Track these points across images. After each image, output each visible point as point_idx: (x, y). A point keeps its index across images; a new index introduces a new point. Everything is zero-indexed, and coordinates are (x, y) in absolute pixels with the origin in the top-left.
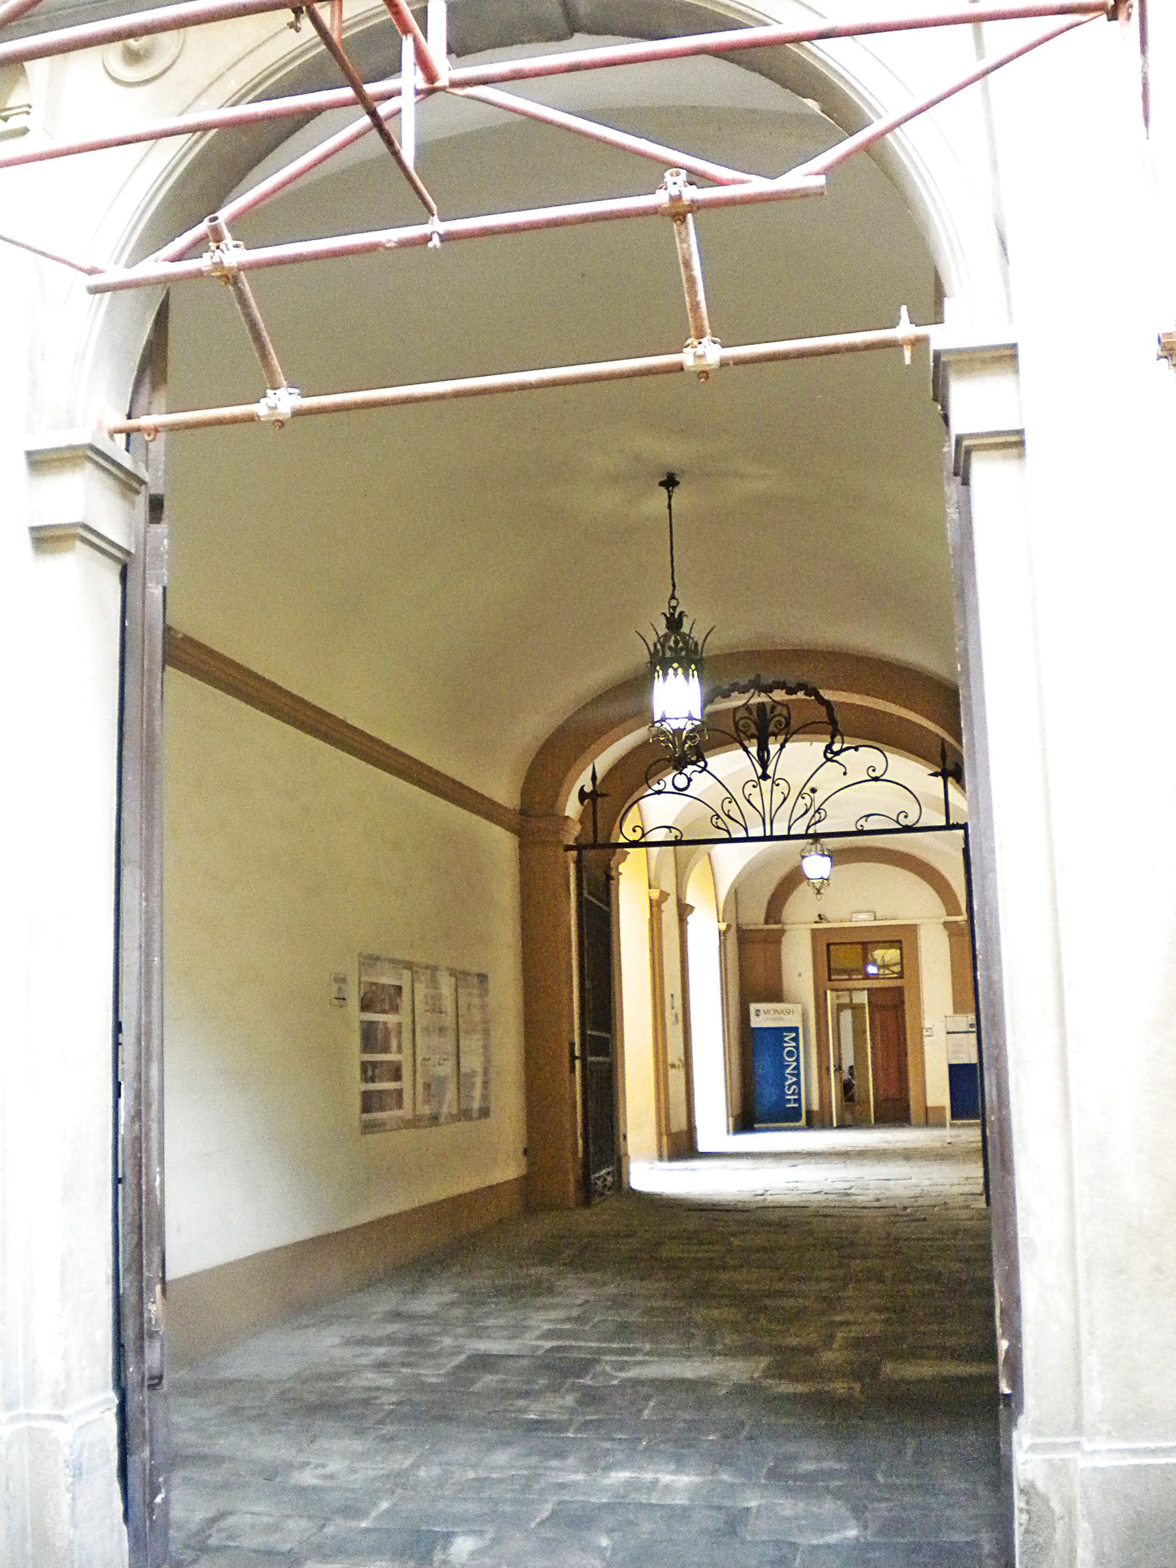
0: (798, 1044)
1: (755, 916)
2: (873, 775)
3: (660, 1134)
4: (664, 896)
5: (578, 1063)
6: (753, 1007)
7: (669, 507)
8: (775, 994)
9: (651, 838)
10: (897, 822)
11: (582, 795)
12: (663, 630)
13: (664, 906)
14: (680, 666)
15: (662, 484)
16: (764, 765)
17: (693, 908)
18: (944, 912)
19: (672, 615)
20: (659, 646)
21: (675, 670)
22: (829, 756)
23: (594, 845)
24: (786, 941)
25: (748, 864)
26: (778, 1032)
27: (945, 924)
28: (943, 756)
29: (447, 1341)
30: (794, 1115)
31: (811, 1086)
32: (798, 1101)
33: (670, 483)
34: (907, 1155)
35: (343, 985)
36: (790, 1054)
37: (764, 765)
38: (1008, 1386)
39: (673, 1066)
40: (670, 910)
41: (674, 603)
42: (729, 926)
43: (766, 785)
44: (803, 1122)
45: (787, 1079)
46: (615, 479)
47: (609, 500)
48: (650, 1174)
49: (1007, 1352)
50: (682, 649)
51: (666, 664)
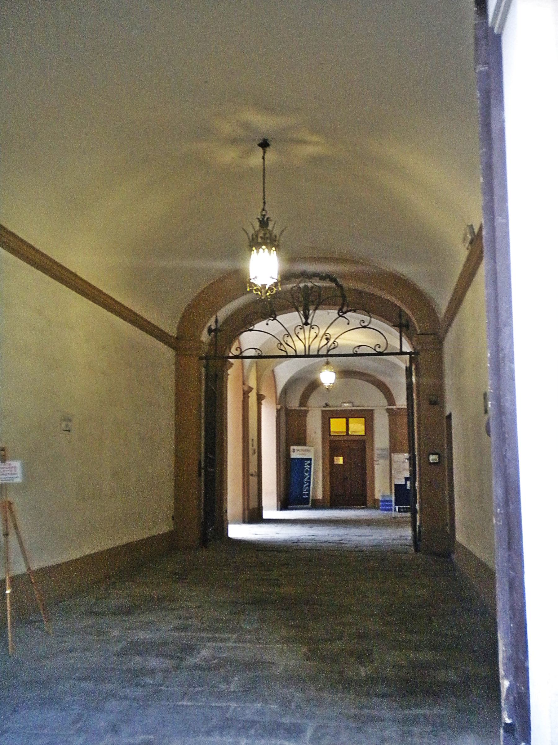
0: (311, 466)
1: (294, 403)
2: (363, 325)
3: (244, 510)
4: (251, 389)
5: (203, 471)
6: (292, 448)
7: (263, 158)
8: (302, 440)
9: (245, 354)
10: (375, 350)
11: (210, 331)
12: (257, 225)
13: (250, 394)
14: (267, 248)
15: (260, 145)
16: (306, 317)
17: (265, 396)
18: (386, 403)
19: (263, 219)
20: (254, 237)
21: (264, 249)
22: (341, 314)
23: (215, 357)
24: (309, 415)
25: (291, 378)
26: (303, 460)
27: (388, 410)
28: (400, 316)
29: (116, 632)
30: (306, 501)
31: (317, 487)
32: (308, 495)
33: (264, 144)
34: (368, 523)
35: (69, 423)
36: (307, 471)
37: (306, 317)
38: (509, 717)
39: (252, 475)
40: (253, 396)
41: (264, 213)
42: (281, 407)
43: (307, 328)
44: (310, 505)
45: (305, 484)
46: (234, 141)
47: (229, 155)
48: (238, 531)
49: (509, 689)
50: (268, 238)
51: (258, 246)
